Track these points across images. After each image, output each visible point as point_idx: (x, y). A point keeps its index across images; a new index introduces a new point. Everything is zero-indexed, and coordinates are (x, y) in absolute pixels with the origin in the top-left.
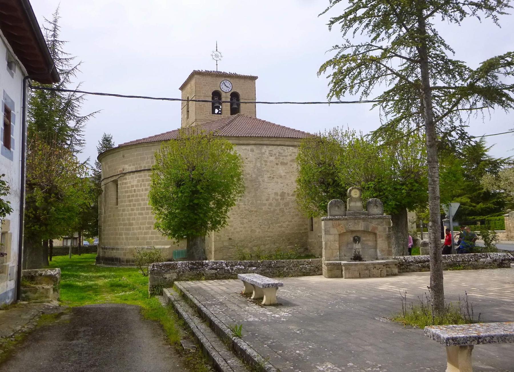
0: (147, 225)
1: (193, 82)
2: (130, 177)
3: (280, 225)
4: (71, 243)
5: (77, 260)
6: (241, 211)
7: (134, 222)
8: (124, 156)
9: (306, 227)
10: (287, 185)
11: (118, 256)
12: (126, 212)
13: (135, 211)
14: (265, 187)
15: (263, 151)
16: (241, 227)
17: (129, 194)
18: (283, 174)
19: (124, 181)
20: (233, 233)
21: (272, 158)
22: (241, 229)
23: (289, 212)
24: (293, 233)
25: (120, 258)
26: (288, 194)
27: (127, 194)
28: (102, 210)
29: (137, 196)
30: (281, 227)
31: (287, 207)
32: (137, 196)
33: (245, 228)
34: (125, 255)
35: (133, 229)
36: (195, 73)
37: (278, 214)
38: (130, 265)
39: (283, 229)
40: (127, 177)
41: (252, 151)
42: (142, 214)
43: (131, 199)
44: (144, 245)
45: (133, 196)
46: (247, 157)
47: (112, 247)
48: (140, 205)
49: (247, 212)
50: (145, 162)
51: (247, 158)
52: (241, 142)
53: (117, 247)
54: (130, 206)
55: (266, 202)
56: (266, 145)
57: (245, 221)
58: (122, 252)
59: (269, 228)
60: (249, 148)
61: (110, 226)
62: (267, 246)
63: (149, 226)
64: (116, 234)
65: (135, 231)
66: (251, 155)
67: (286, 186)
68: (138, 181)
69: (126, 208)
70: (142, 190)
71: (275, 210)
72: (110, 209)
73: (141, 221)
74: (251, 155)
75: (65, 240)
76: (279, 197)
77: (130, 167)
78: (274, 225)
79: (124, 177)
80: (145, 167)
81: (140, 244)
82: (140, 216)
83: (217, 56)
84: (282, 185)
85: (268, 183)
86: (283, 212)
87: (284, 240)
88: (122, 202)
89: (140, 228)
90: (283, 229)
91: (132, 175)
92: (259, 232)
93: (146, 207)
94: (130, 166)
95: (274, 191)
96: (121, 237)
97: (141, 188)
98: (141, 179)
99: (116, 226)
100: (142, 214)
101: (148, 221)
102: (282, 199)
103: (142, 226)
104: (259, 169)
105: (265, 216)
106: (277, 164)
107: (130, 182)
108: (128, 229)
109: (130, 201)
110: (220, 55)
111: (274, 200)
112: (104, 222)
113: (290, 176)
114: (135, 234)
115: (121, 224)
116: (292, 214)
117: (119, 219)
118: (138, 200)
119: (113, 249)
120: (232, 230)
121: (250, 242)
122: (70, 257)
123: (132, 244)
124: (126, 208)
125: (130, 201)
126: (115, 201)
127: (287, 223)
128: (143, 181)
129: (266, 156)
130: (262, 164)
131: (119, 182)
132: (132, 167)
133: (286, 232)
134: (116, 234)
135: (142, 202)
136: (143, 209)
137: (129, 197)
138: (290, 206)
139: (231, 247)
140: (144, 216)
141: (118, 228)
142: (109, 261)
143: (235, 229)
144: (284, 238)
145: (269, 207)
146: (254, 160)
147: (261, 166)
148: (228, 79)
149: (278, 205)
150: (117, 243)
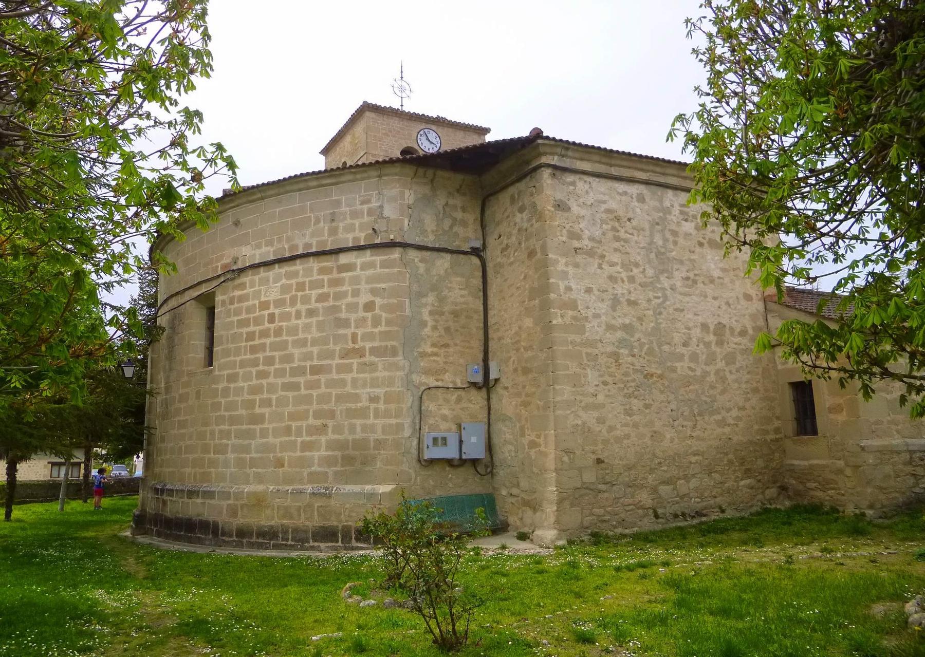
0: (311, 421)
1: (359, 129)
2: (256, 278)
3: (719, 417)
4: (66, 474)
5: (81, 518)
6: (626, 374)
7: (266, 411)
8: (237, 223)
9: (777, 424)
10: (728, 304)
11: (209, 515)
12: (241, 384)
13: (271, 380)
14: (678, 306)
15: (667, 204)
16: (626, 425)
17: (251, 329)
18: (716, 273)
19: (237, 293)
20: (606, 442)
21: (689, 227)
22: (627, 430)
23: (736, 381)
24: (751, 442)
25: (216, 525)
26: (732, 329)
27: (244, 330)
28: (158, 380)
29: (278, 332)
30: (722, 423)
31: (733, 368)
32: (278, 332)
33: (636, 425)
34: (234, 514)
35: (264, 433)
36: (366, 108)
37: (713, 387)
38: (252, 545)
39: (727, 430)
40: (246, 279)
41: (641, 199)
42: (295, 387)
43: (257, 342)
44: (301, 481)
45: (264, 334)
46: (630, 215)
47: (188, 486)
48: (288, 359)
49: (639, 377)
50: (308, 232)
51: (629, 220)
52: (614, 171)
53: (205, 487)
54: (255, 363)
55: (684, 350)
56: (675, 188)
57: (636, 404)
58: (225, 503)
59: (695, 426)
60: (634, 189)
61: (182, 425)
62: (694, 483)
63: (318, 422)
64: (206, 449)
65: (271, 440)
66: (638, 210)
67: (724, 307)
68: (285, 289)
69: (241, 371)
70: (298, 315)
71: (706, 374)
72: (185, 379)
73: (290, 408)
74: (638, 210)
75: (56, 468)
76: (711, 338)
77: (258, 252)
78: (706, 418)
79: (237, 282)
80: (308, 245)
81: (288, 480)
82: (290, 394)
83: (402, 85)
84: (716, 303)
85: (685, 294)
86: (723, 379)
87: (731, 462)
88: (227, 353)
89: (288, 431)
90: (727, 430)
91: (263, 273)
92: (672, 440)
93: (308, 364)
94: (258, 246)
95: (700, 319)
96: (221, 457)
97: (293, 310)
98: (293, 281)
99: (206, 424)
100: (295, 387)
101: (315, 406)
102: (720, 343)
103: (294, 425)
104: (663, 254)
105: (682, 391)
106: (701, 244)
107: (257, 294)
108: (250, 435)
109: (254, 350)
110: (408, 88)
111: (701, 346)
112: (165, 416)
113: (732, 282)
114: (267, 448)
115: (220, 420)
116: (744, 386)
117: (216, 406)
118: (283, 346)
119: (192, 494)
120: (604, 431)
121: (652, 471)
122: (62, 509)
123: (260, 479)
124: (241, 371)
125: (254, 350)
126: (201, 354)
127: (735, 413)
128: (301, 287)
129: (674, 219)
130: (666, 240)
131: (219, 298)
132: (264, 249)
133: (735, 439)
134: (206, 449)
135: (297, 352)
136: (300, 371)
137: (251, 336)
138: (738, 365)
139: (603, 487)
140: (303, 392)
141: (212, 433)
142: (177, 528)
143: (611, 429)
144: (731, 456)
145: (692, 365)
146: (647, 226)
147: (664, 246)
148: (433, 127)
149: (711, 359)
150: (206, 477)
